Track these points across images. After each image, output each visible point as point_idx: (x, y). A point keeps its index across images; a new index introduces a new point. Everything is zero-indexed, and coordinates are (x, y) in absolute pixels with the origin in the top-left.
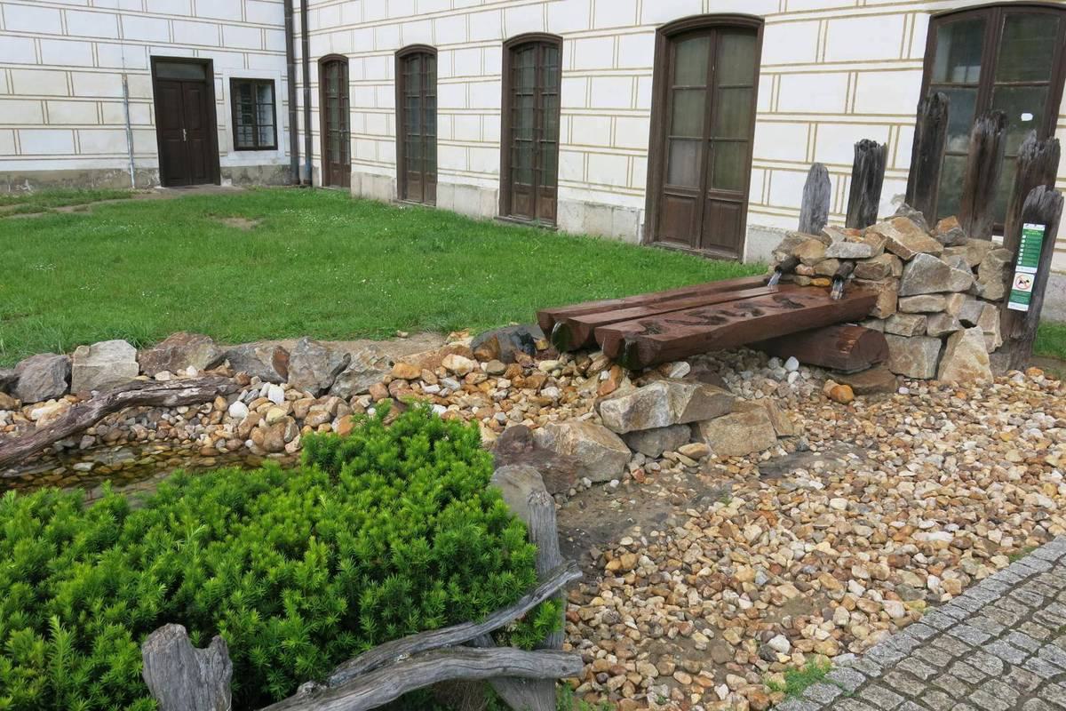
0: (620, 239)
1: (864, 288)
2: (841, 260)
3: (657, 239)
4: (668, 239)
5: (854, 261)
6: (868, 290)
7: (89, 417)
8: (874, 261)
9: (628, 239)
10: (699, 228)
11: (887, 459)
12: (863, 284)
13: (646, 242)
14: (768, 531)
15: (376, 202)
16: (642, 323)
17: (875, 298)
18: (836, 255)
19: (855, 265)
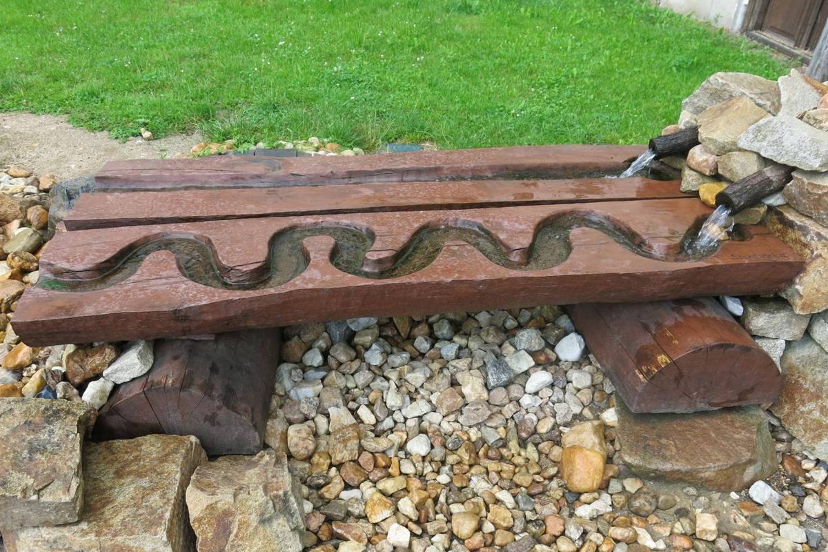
0: (716, 20)
1: (792, 235)
2: (766, 161)
3: (759, 27)
4: (773, 29)
5: (788, 172)
6: (797, 241)
7: (579, 464)
8: (819, 181)
9: (722, 23)
10: (811, 21)
11: (270, 37)
12: (791, 225)
13: (745, 30)
14: (330, 370)
15: (175, 312)
16: (598, 191)
17: (799, 268)
18: (756, 146)
19: (789, 178)
